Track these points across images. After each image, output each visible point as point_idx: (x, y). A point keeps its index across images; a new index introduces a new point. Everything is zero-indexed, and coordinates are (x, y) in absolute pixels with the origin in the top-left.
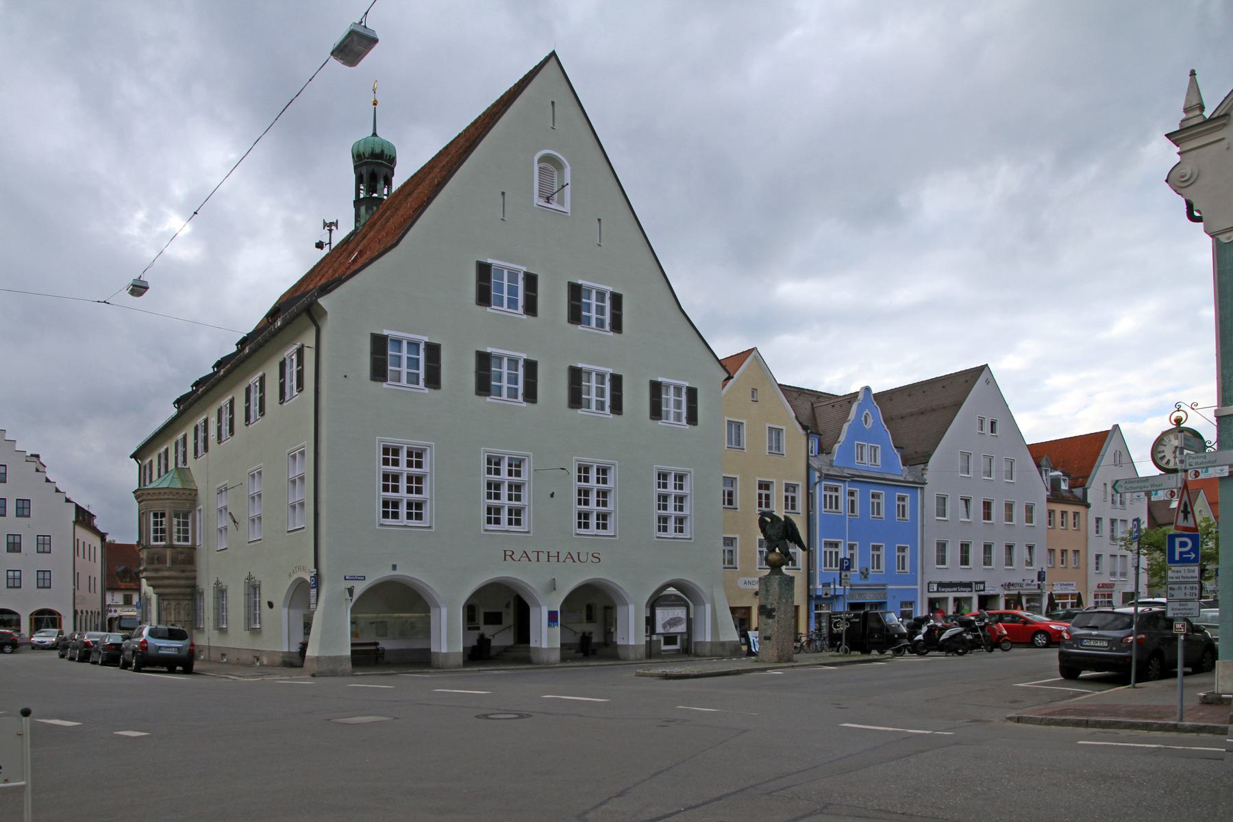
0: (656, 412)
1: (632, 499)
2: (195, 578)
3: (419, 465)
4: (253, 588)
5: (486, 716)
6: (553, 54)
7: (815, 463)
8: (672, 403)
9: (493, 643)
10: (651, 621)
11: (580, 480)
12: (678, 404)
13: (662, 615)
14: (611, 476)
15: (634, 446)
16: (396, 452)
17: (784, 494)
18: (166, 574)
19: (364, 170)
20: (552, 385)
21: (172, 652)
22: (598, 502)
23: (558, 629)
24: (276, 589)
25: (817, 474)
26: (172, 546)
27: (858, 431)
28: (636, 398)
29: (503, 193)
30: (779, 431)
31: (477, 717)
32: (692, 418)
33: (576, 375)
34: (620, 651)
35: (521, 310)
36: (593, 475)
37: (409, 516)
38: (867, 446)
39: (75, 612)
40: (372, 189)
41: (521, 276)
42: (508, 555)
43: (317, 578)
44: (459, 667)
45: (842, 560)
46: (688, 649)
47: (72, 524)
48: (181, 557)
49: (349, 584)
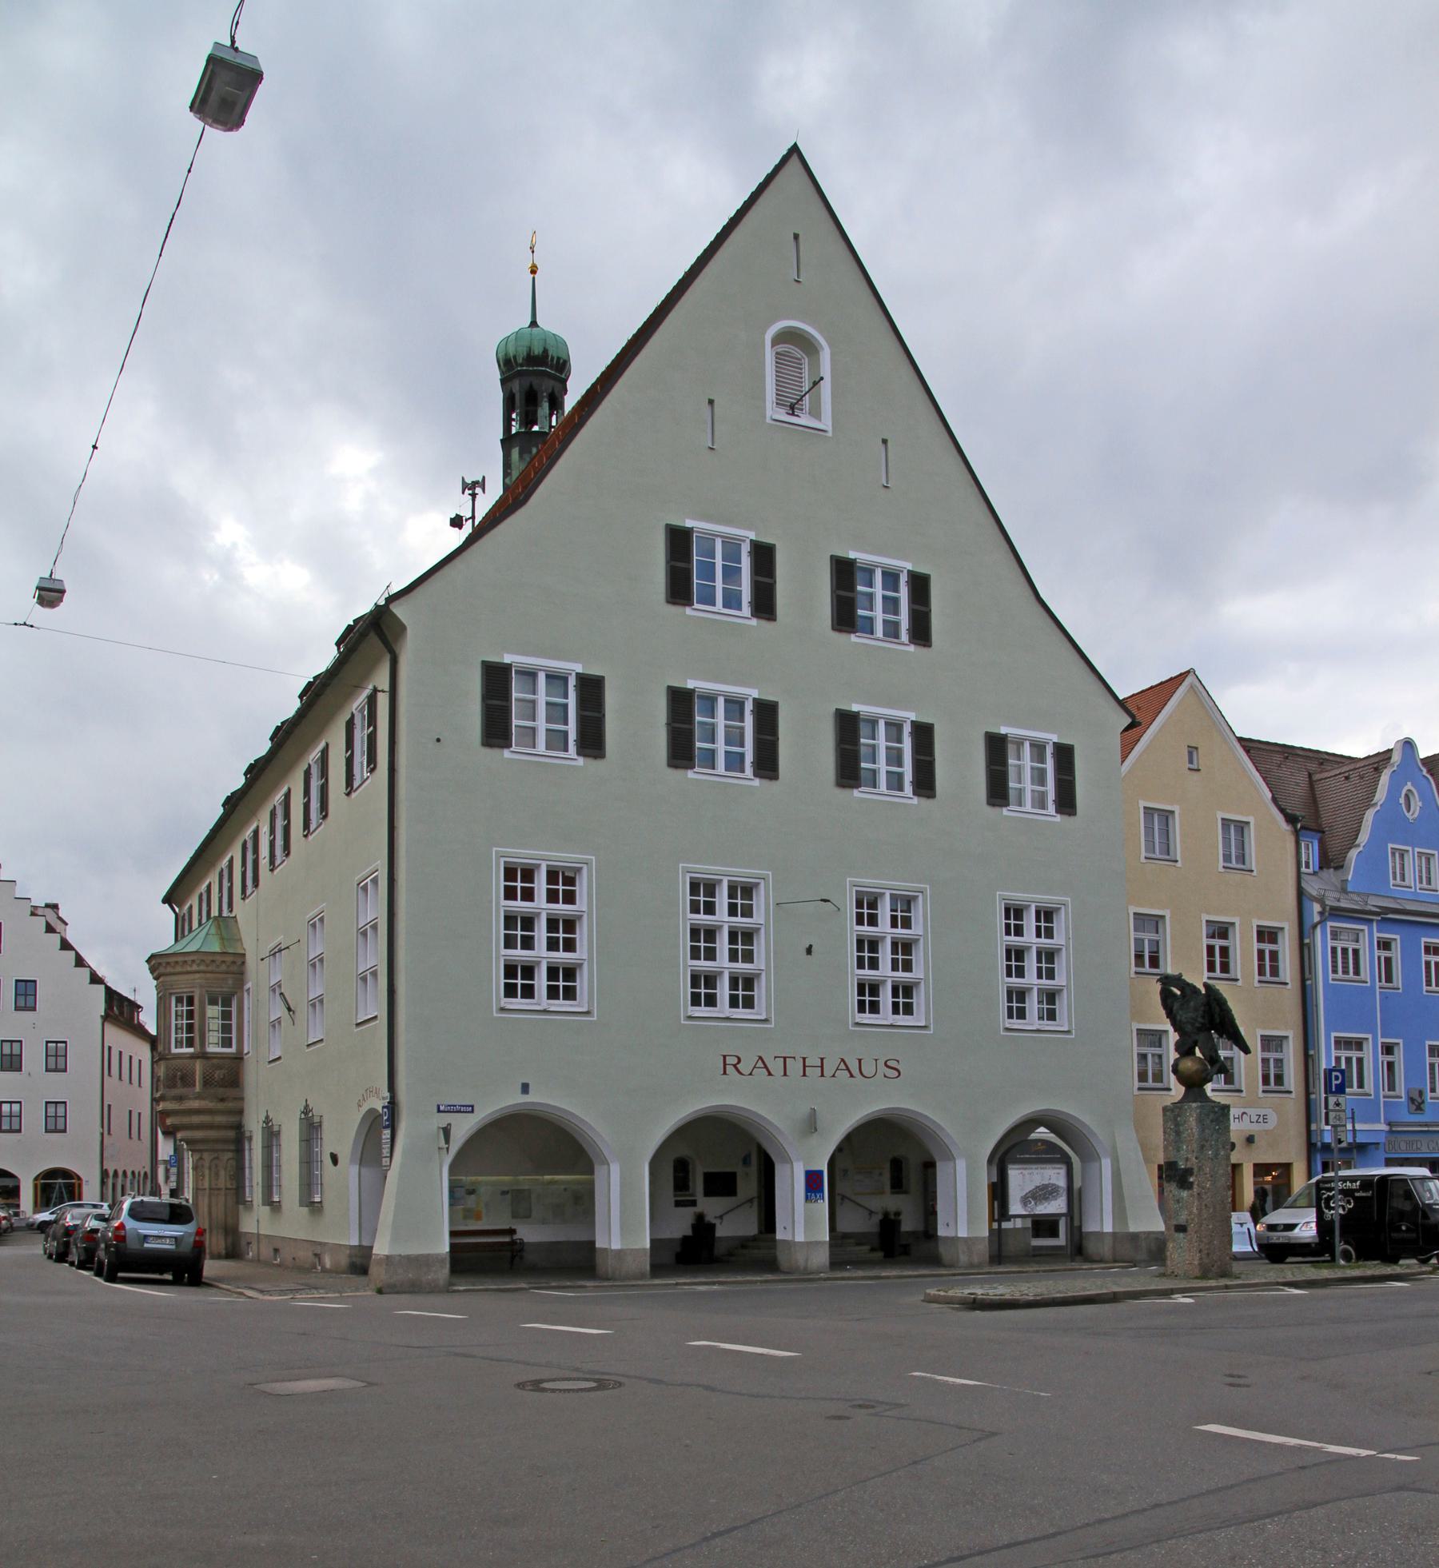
0: (998, 792)
1: (956, 955)
2: (241, 1112)
3: (570, 898)
4: (311, 1128)
5: (536, 1385)
6: (795, 150)
7: (1312, 887)
8: (1027, 775)
9: (721, 1231)
10: (999, 1192)
11: (860, 922)
12: (1040, 777)
13: (1021, 1180)
14: (1059, 924)
15: (956, 856)
16: (529, 874)
17: (1256, 946)
18: (195, 1104)
19: (516, 386)
20: (807, 746)
21: (168, 1246)
22: (895, 962)
23: (824, 1206)
24: (341, 1135)
25: (1317, 907)
26: (203, 1056)
27: (1393, 825)
28: (960, 766)
29: (711, 402)
30: (1242, 827)
31: (521, 1386)
32: (1066, 802)
33: (848, 726)
34: (942, 1249)
35: (746, 610)
36: (1030, 922)
37: (553, 993)
38: (1412, 853)
39: (104, 1174)
40: (529, 419)
41: (745, 549)
42: (730, 1064)
43: (393, 1106)
44: (642, 1276)
45: (1328, 1073)
46: (1079, 1249)
47: (100, 1021)
48: (219, 1074)
49: (445, 1119)
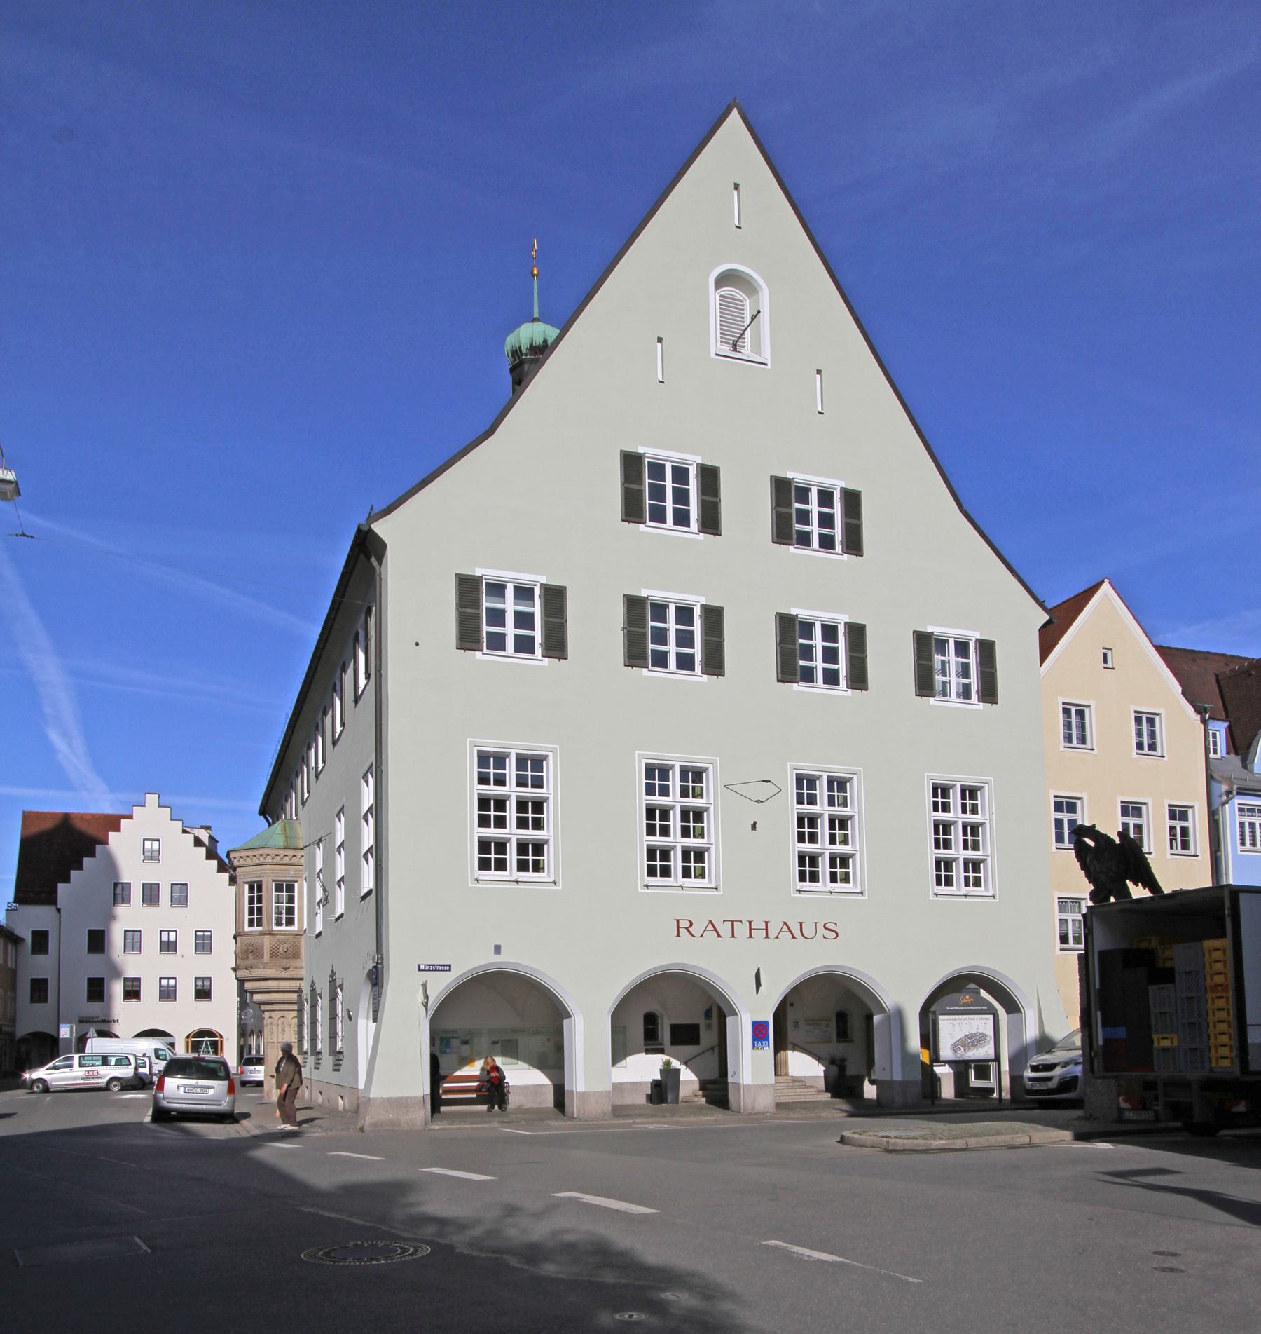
11: (937, 846)
26: (271, 933)
37: (522, 866)
42: (683, 928)
